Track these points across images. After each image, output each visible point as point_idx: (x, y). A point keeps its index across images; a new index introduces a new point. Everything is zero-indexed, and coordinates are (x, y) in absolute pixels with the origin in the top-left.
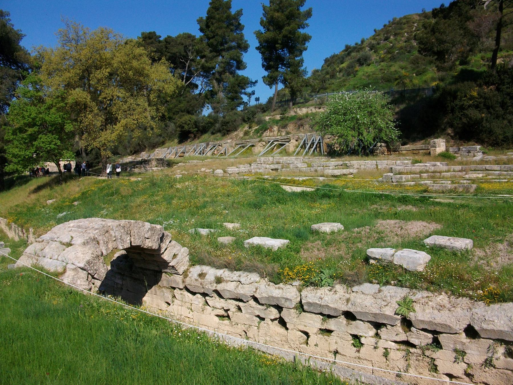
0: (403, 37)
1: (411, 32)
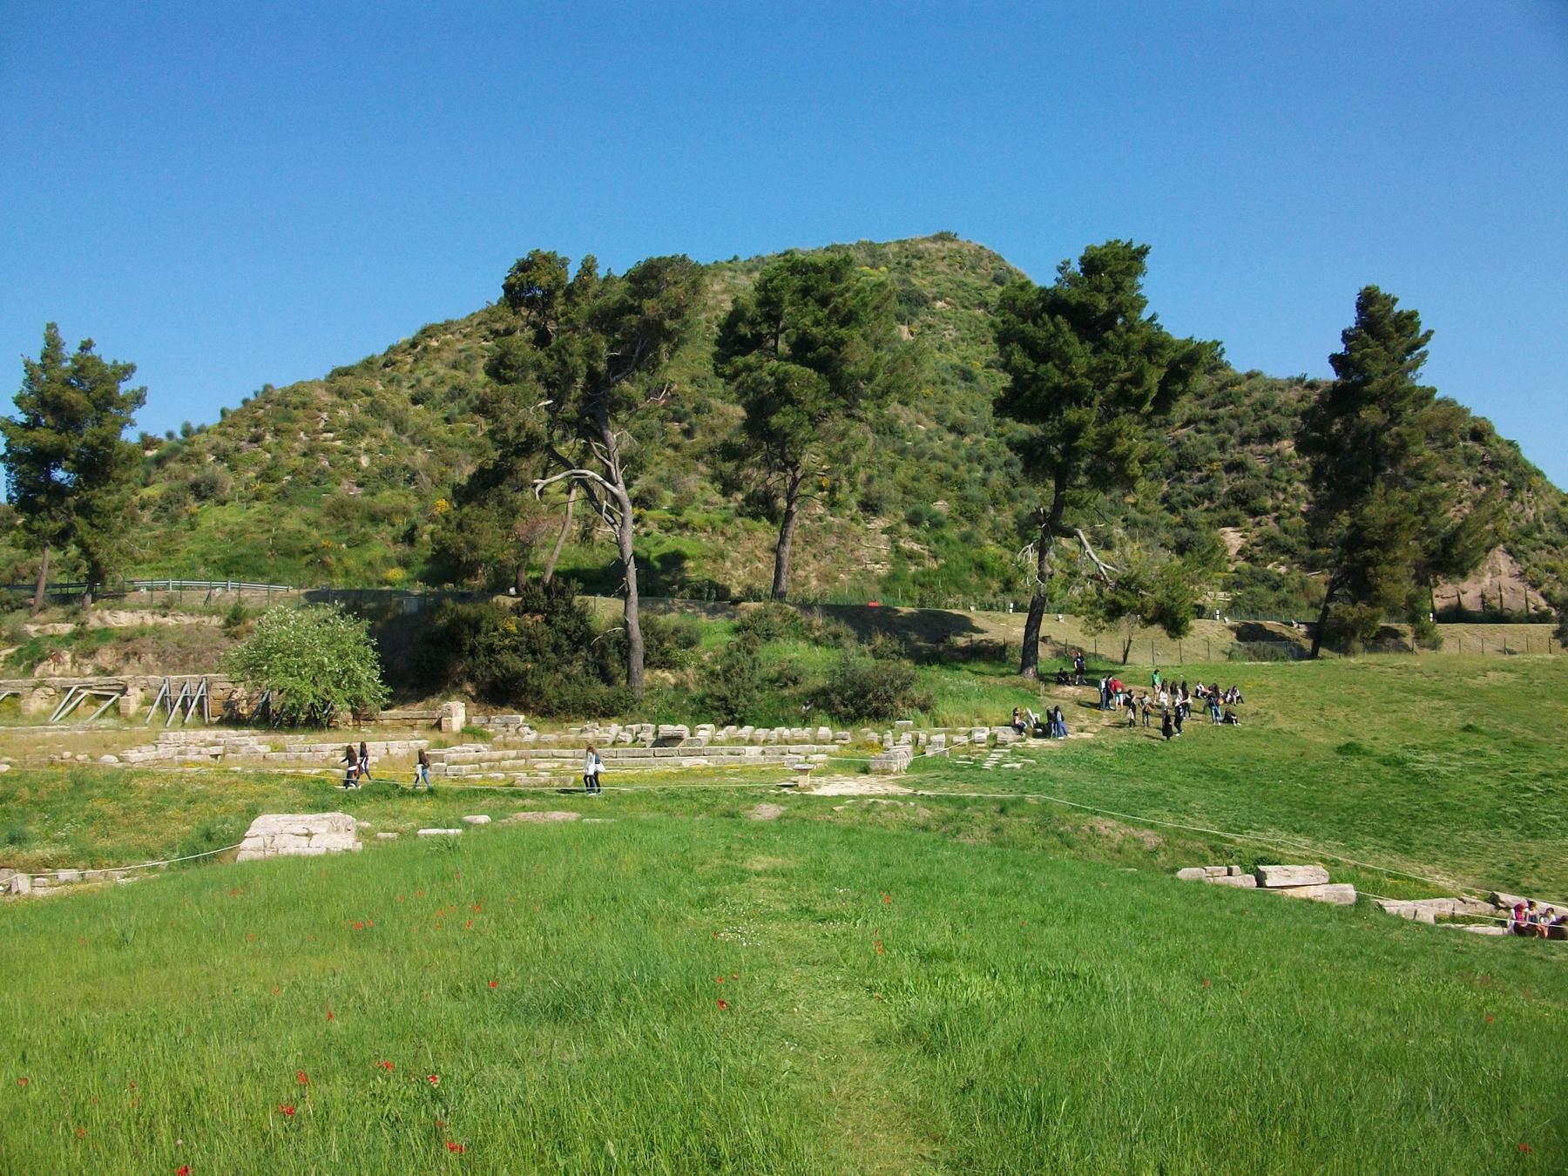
0: (295, 440)
1: (315, 432)
